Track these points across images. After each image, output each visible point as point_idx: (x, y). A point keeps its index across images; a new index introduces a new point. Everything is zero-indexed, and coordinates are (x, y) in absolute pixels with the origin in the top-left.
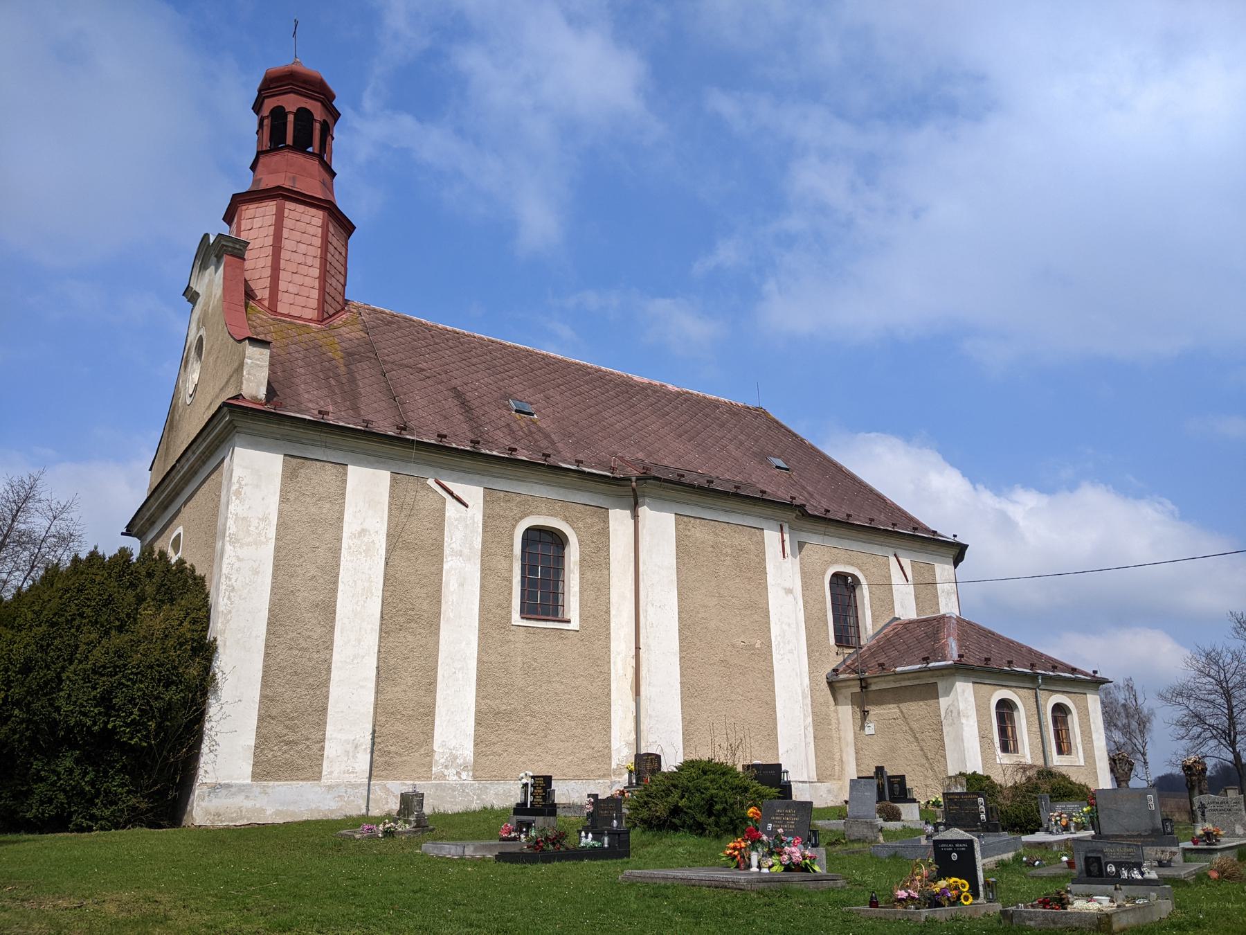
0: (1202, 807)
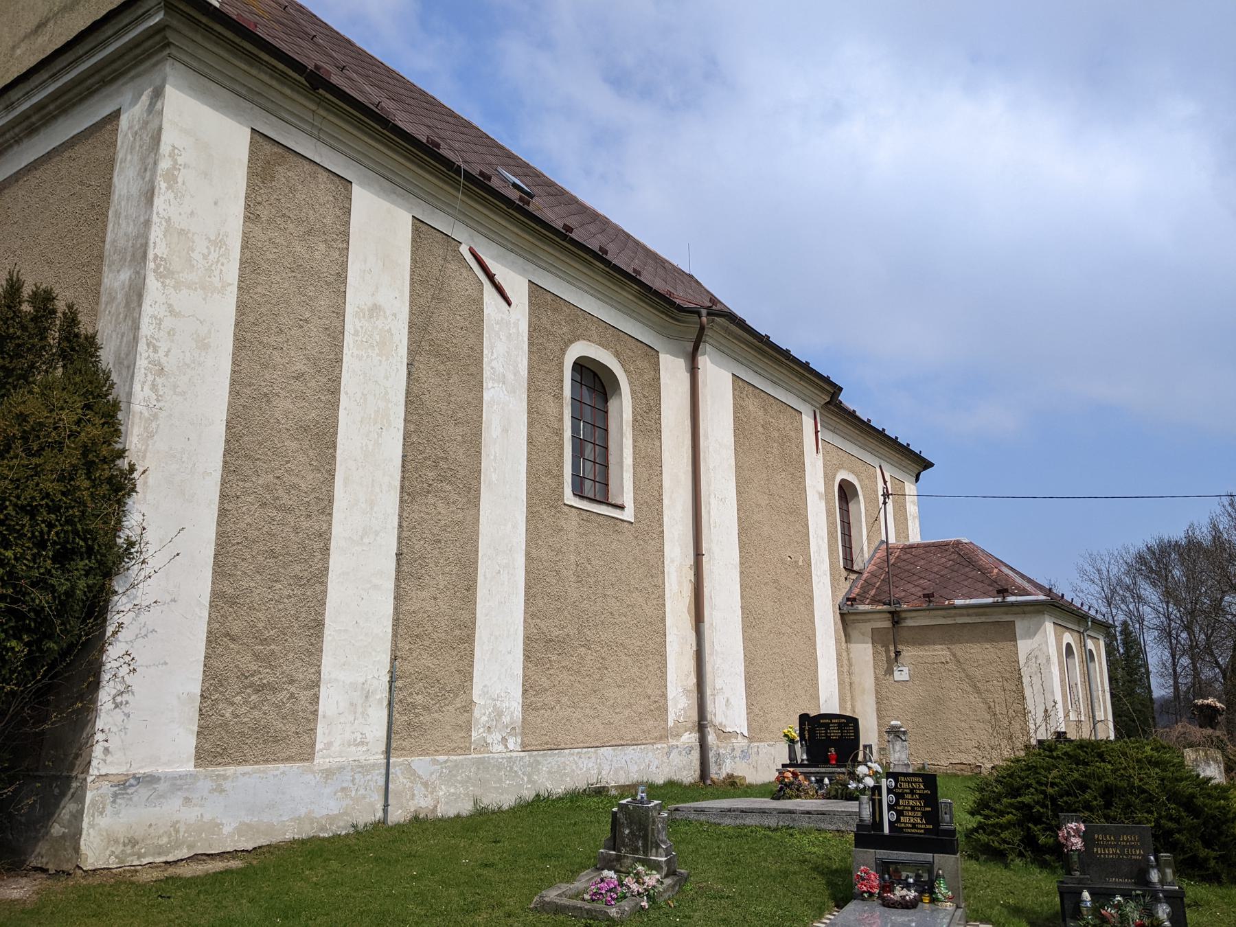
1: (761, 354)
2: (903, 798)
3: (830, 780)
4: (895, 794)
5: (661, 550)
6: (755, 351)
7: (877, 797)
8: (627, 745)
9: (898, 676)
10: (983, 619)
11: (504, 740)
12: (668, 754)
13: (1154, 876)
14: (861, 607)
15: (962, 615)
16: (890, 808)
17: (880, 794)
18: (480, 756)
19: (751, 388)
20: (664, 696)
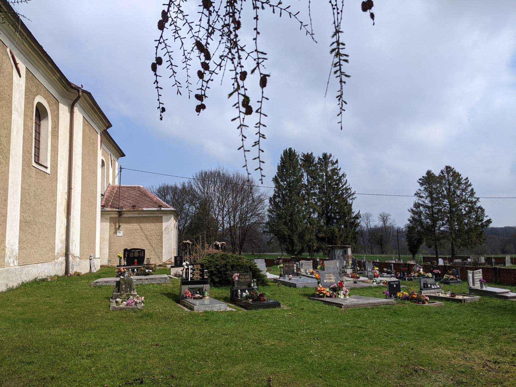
0: (302, 264)
1: (92, 109)
2: (195, 271)
3: (137, 270)
4: (192, 270)
5: (56, 186)
6: (91, 108)
7: (187, 271)
8: (45, 262)
9: (118, 234)
10: (152, 215)
11: (14, 262)
12: (55, 265)
13: (252, 285)
14: (107, 209)
15: (145, 214)
16: (191, 273)
17: (189, 270)
18: (8, 268)
19: (87, 122)
20: (54, 243)
